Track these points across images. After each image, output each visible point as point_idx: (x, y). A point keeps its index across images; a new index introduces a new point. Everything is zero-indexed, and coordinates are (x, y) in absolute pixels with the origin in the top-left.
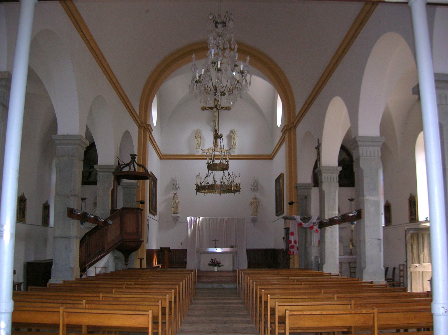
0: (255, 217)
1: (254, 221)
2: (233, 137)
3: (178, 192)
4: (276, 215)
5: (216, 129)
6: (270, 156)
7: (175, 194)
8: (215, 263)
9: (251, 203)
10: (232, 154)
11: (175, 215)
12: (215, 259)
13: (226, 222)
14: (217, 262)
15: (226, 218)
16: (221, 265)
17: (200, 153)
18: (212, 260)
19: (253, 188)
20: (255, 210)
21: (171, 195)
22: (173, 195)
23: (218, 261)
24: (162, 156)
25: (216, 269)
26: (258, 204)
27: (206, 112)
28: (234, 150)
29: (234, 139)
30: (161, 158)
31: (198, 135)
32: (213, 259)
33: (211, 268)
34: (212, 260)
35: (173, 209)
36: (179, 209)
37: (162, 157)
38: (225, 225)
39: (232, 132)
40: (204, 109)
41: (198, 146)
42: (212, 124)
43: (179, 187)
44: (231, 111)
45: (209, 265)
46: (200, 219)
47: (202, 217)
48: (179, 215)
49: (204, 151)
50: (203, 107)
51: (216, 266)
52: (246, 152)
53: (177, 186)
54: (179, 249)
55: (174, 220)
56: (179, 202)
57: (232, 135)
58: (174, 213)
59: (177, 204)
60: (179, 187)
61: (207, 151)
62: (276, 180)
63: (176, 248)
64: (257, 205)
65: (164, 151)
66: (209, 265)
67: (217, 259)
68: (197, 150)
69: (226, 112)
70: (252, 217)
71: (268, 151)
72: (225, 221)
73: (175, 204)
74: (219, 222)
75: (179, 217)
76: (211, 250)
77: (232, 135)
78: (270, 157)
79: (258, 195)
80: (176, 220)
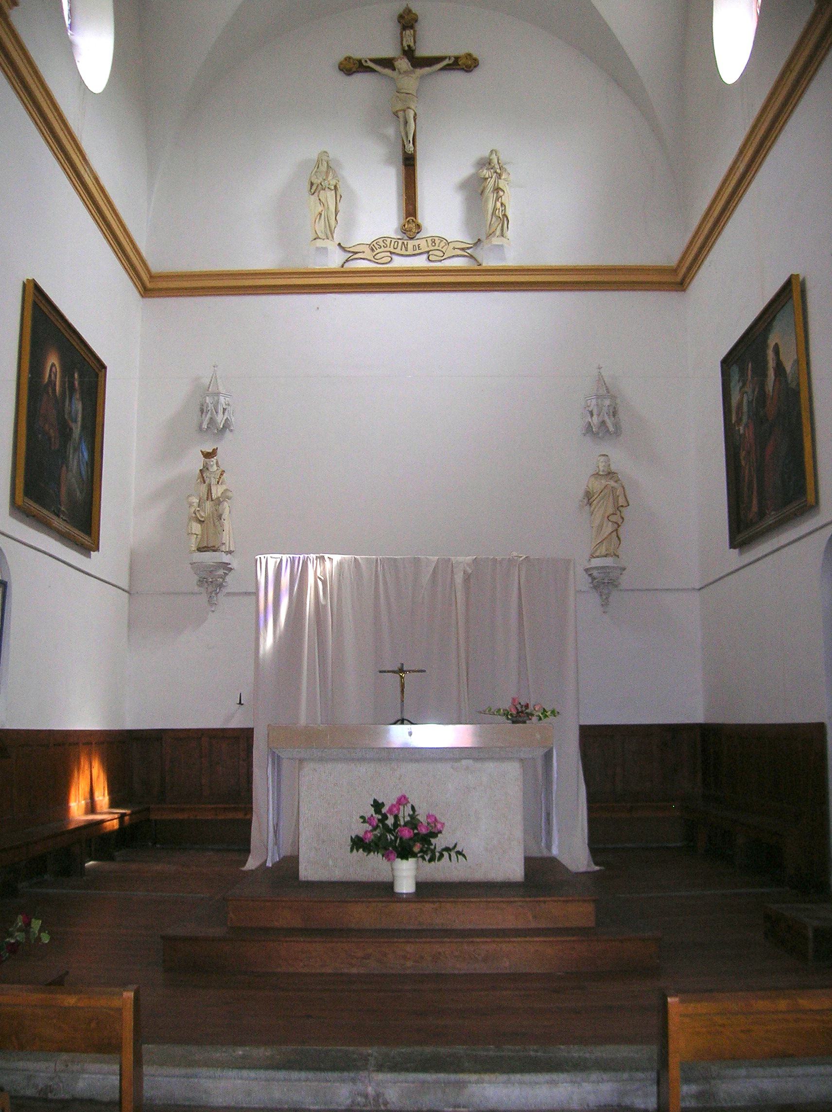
0: (609, 562)
1: (604, 583)
2: (491, 183)
3: (226, 447)
4: (732, 545)
5: (410, 148)
6: (674, 271)
7: (208, 455)
8: (398, 833)
9: (589, 496)
10: (490, 261)
11: (208, 557)
12: (402, 800)
13: (467, 578)
14: (413, 822)
15: (464, 559)
16: (439, 843)
17: (334, 260)
18: (377, 806)
19: (595, 420)
20: (609, 528)
21: (194, 462)
22: (200, 462)
23: (422, 818)
24: (152, 277)
25: (406, 875)
26: (622, 501)
27: (360, 80)
28: (496, 241)
29: (497, 189)
30: (146, 291)
31: (322, 180)
32: (389, 800)
33: (372, 867)
34: (377, 806)
35: (196, 528)
36: (227, 524)
37: (151, 285)
38: (460, 595)
39: (485, 163)
40: (352, 67)
41: (320, 227)
42: (391, 131)
43: (227, 426)
44: (477, 73)
45: (358, 843)
46: (326, 567)
47: (337, 558)
48: (226, 558)
49: (353, 254)
50: (348, 59)
51: (405, 853)
52: (554, 255)
53: (220, 419)
54: (826, 759)
55: (202, 582)
56: (225, 496)
57: (486, 173)
58: (200, 550)
59: (218, 502)
60: (227, 426)
61: (368, 254)
62: (727, 363)
63: (218, 727)
64: (618, 508)
65: (159, 261)
66: (358, 843)
67: (413, 799)
68: (319, 243)
69: (457, 77)
70: (596, 562)
71: (664, 249)
72: (459, 578)
73: (208, 505)
74: (426, 578)
75: (226, 566)
76: (400, 735)
77: (486, 173)
78: (676, 279)
79: (620, 459)
80: (212, 581)
